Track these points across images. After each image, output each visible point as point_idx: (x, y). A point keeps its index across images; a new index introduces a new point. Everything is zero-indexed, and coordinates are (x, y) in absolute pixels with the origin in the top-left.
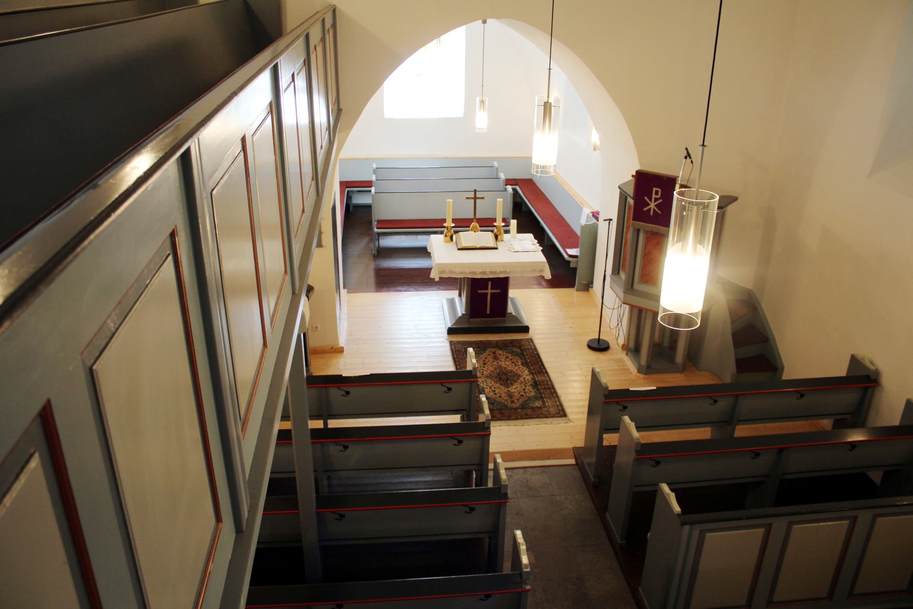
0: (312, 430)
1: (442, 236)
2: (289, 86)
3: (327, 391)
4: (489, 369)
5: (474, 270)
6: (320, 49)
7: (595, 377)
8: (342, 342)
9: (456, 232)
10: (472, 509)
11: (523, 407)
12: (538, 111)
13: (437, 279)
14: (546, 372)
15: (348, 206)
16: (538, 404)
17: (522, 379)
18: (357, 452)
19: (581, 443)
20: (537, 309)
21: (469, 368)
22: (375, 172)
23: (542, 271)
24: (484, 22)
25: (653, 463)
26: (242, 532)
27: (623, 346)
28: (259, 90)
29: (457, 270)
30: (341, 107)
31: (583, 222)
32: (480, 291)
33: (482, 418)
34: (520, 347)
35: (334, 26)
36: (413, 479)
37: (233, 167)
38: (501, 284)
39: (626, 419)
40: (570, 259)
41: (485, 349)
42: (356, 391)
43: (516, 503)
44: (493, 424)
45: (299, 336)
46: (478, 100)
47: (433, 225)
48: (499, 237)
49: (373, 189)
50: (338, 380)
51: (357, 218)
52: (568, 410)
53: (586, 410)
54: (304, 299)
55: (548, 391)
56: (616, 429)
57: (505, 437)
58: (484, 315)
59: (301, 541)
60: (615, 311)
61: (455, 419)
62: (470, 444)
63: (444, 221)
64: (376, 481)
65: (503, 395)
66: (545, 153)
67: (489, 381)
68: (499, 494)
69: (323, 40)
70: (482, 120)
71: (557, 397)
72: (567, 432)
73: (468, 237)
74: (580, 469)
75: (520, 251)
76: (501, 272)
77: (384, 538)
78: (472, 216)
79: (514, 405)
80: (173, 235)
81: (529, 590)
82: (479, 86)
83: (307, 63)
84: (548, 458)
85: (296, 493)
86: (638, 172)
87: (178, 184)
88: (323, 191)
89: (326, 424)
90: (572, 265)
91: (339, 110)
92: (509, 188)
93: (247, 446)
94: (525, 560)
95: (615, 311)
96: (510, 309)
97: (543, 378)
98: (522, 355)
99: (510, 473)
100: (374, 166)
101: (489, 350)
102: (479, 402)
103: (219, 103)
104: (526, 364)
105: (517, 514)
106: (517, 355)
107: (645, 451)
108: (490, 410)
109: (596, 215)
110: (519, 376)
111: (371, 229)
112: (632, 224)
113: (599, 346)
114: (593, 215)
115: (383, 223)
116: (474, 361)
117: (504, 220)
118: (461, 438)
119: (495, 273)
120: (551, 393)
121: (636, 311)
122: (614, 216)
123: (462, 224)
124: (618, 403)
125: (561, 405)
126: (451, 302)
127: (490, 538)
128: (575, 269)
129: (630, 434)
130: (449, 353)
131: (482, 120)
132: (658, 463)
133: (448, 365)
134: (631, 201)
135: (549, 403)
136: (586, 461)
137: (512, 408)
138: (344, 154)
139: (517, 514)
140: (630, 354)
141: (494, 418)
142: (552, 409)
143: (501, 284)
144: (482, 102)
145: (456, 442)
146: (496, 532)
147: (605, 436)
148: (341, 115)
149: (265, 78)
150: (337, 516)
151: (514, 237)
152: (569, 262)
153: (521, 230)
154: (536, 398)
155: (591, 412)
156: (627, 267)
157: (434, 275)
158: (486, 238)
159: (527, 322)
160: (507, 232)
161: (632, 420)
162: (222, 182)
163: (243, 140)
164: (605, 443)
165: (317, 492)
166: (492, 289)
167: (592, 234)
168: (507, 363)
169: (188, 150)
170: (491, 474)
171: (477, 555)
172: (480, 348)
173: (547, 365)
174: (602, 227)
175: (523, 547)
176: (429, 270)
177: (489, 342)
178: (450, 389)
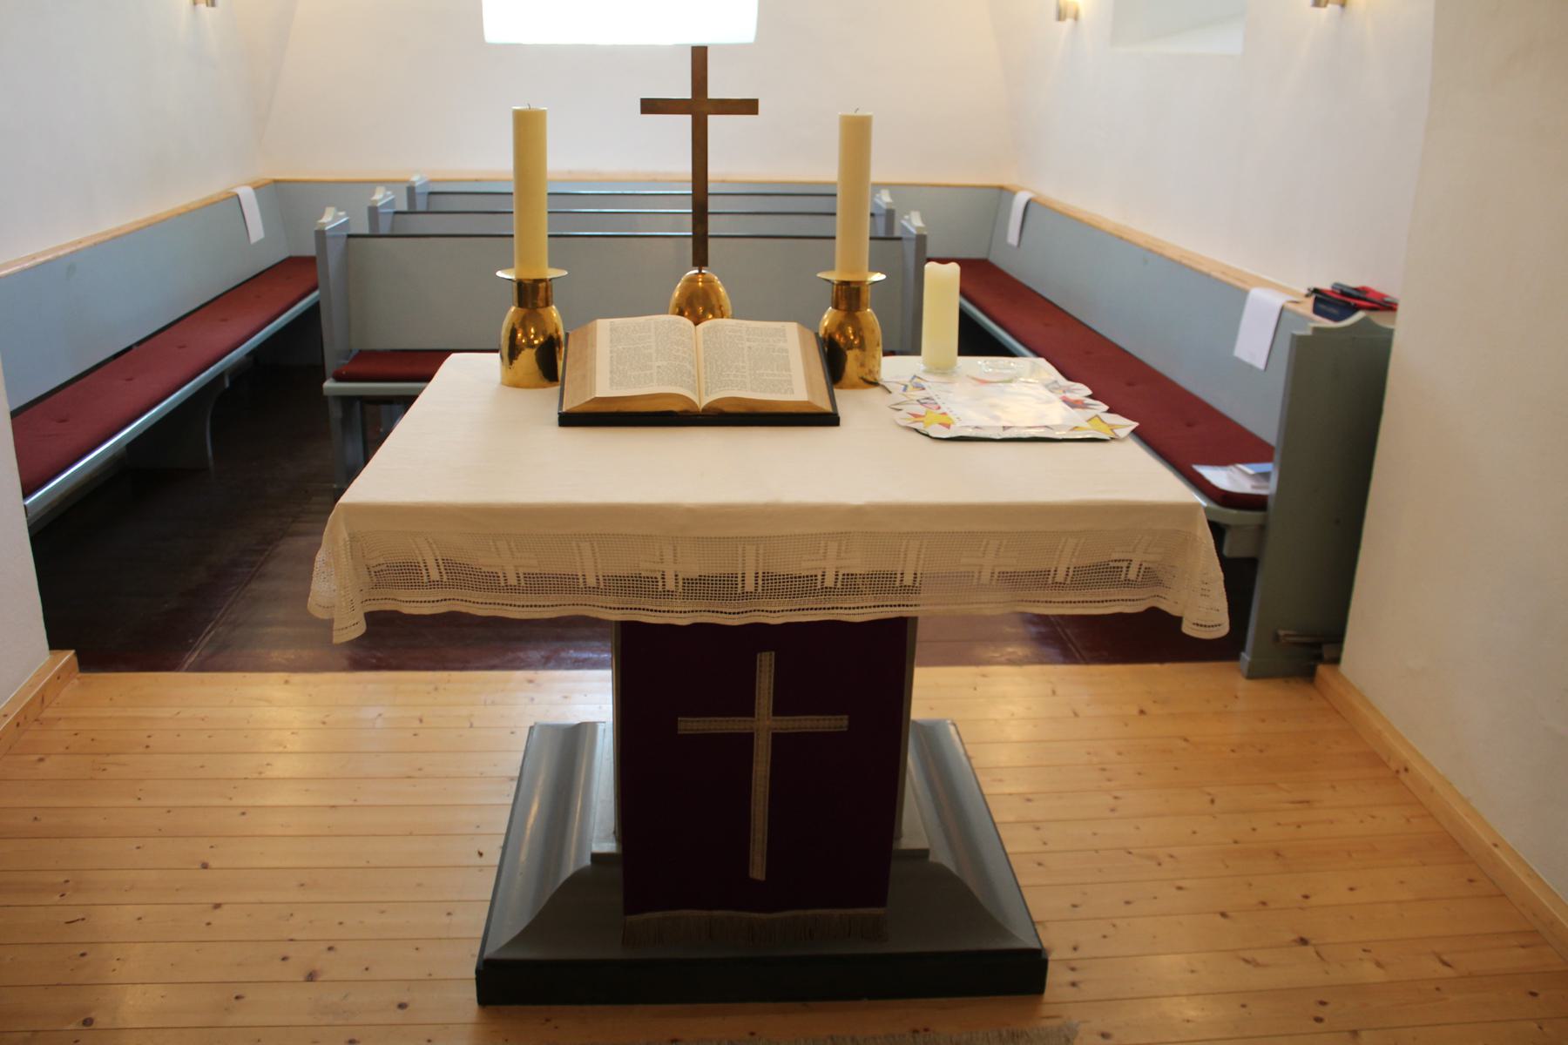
5: (646, 566)
29: (509, 563)
32: (690, 725)
76: (850, 584)
96: (916, 824)
119: (805, 585)
151: (942, 370)
160: (908, 344)
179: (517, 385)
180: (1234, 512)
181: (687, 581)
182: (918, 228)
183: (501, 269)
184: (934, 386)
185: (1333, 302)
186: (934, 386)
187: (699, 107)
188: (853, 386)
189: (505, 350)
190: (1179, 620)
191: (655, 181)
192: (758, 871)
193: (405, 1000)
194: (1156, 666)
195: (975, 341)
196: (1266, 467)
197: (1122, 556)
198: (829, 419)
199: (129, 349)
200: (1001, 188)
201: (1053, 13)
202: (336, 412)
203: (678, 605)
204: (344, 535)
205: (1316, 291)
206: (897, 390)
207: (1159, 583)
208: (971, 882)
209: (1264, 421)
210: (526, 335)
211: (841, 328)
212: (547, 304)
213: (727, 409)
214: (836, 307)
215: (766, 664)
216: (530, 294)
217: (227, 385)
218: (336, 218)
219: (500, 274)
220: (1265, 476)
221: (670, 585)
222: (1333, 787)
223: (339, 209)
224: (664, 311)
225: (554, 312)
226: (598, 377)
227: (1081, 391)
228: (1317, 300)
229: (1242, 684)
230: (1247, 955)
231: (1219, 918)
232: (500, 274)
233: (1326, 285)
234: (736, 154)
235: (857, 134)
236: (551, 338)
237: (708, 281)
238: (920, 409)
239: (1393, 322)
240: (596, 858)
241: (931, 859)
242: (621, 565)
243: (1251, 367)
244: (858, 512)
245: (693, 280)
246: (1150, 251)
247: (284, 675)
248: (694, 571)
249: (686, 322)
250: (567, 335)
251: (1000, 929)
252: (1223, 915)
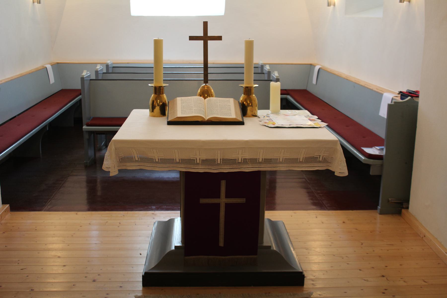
5: (191, 156)
32: (203, 201)
40: (370, 161)
76: (245, 161)
90: (373, 172)
96: (268, 239)
119: (233, 162)
152: (368, 166)
160: (267, 107)
166: (228, 196)
179: (154, 116)
180: (372, 160)
181: (203, 160)
182: (277, 76)
183: (150, 84)
184: (272, 116)
185: (403, 95)
186: (272, 116)
187: (205, 38)
188: (249, 117)
189: (151, 106)
190: (334, 172)
191: (190, 63)
192: (221, 244)
193: (122, 286)
194: (351, 211)
195: (286, 105)
196: (383, 147)
197: (317, 154)
198: (242, 123)
199: (15, 117)
200: (311, 65)
201: (326, 4)
202: (86, 136)
203: (200, 167)
204: (113, 148)
205: (401, 92)
206: (262, 118)
207: (328, 162)
208: (283, 255)
209: (381, 132)
210: (157, 102)
211: (246, 100)
212: (163, 94)
213: (213, 120)
214: (244, 94)
215: (223, 184)
216: (158, 91)
217: (48, 129)
218: (87, 74)
219: (149, 85)
220: (383, 149)
221: (198, 162)
222: (401, 241)
223: (88, 71)
224: (196, 95)
225: (165, 96)
226: (178, 112)
227: (315, 117)
228: (401, 95)
229: (378, 216)
230: (366, 279)
231: (359, 271)
232: (149, 85)
233: (404, 90)
234: (219, 55)
235: (250, 46)
236: (164, 103)
237: (208, 87)
238: (267, 121)
239: (418, 100)
241: (272, 248)
242: (185, 156)
243: (384, 118)
244: (247, 142)
245: (204, 87)
246: (356, 83)
247: (76, 212)
248: (204, 157)
249: (202, 98)
250: (168, 102)
251: (291, 267)
252: (360, 270)
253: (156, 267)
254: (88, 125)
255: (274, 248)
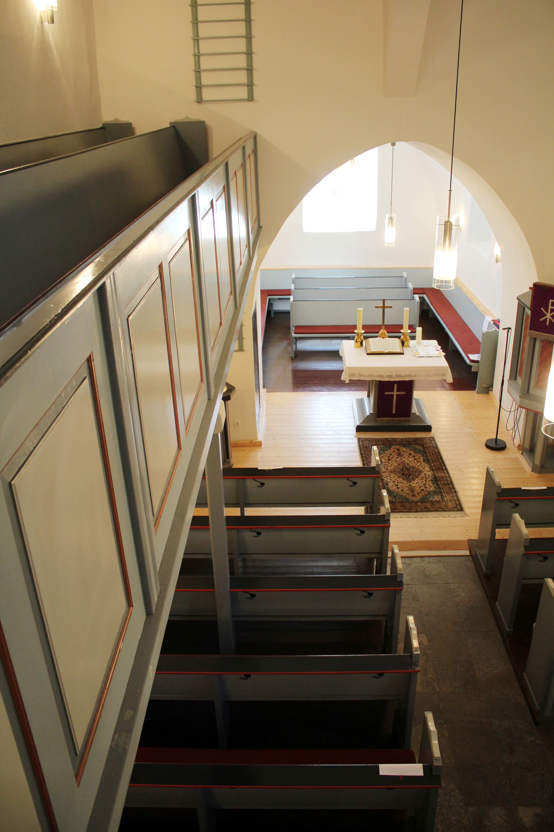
0: (228, 517)
1: (353, 341)
2: (207, 212)
3: (244, 481)
4: (393, 464)
6: (240, 175)
7: (489, 476)
8: (260, 437)
9: (366, 338)
10: (370, 594)
11: (423, 501)
12: (438, 231)
13: (347, 381)
14: (446, 469)
15: (269, 312)
16: (437, 498)
17: (423, 475)
18: (268, 537)
19: (475, 537)
20: (440, 409)
21: (373, 464)
22: (294, 281)
23: (444, 375)
24: (393, 144)
25: (542, 559)
26: (152, 614)
27: (519, 446)
28: (179, 219)
29: (366, 374)
30: (261, 224)
31: (485, 329)
32: (386, 393)
33: (383, 511)
34: (422, 445)
35: (255, 151)
36: (319, 564)
37: (150, 293)
38: (407, 387)
39: (517, 516)
40: (472, 364)
41: (390, 446)
42: (270, 483)
43: (411, 588)
44: (392, 516)
45: (215, 436)
46: (387, 217)
47: (345, 331)
48: (406, 344)
49: (291, 298)
50: (254, 473)
51: (276, 323)
52: (464, 505)
53: (481, 505)
54: (219, 402)
55: (447, 486)
56: (507, 525)
57: (404, 528)
58: (391, 415)
59: (216, 616)
60: (512, 414)
61: (359, 511)
62: (371, 535)
63: (355, 327)
64: (286, 564)
65: (405, 489)
66: (445, 269)
67: (392, 476)
68: (395, 582)
69: (243, 166)
70: (390, 236)
71: (455, 492)
72: (462, 526)
73: (377, 343)
74: (473, 560)
75: (426, 355)
76: (406, 376)
77: (287, 616)
78: (380, 323)
79: (415, 499)
80: (89, 360)
81: (418, 671)
82: (389, 203)
83: (227, 190)
84: (445, 549)
85: (212, 573)
86: (535, 285)
87: (94, 315)
88: (241, 305)
89: (242, 512)
91: (260, 228)
92: (417, 297)
93: (157, 542)
94: (415, 643)
95: (512, 414)
96: (414, 409)
97: (442, 474)
98: (424, 453)
99: (407, 561)
100: (294, 276)
101: (393, 447)
102: (381, 494)
103: (124, 248)
104: (427, 461)
105: (414, 599)
106: (420, 452)
107: (533, 545)
108: (391, 502)
109: (496, 323)
110: (421, 472)
111: (289, 333)
112: (529, 334)
113: (496, 446)
114: (494, 323)
115: (301, 329)
116: (378, 458)
117: (411, 327)
118: (363, 529)
119: (400, 376)
120: (450, 489)
121: (531, 415)
122: (512, 324)
123: (372, 330)
124: (510, 501)
125: (458, 500)
126: (360, 402)
127: (386, 621)
128: (476, 373)
129: (520, 531)
130: (357, 449)
131: (390, 236)
132: (546, 558)
133: (356, 462)
134: (528, 312)
135: (447, 497)
136: (479, 552)
137: (412, 502)
138: (264, 265)
139: (414, 599)
140: (525, 454)
141: (394, 509)
142: (449, 504)
143: (407, 387)
144: (391, 218)
145: (358, 532)
146: (392, 615)
147: (497, 530)
148: (261, 231)
149: (184, 208)
150: (249, 596)
151: (419, 344)
152: (470, 367)
153: (426, 336)
154: (435, 493)
155: (485, 507)
156: (523, 373)
157: (345, 377)
158: (394, 344)
159: (429, 420)
160: (413, 338)
161: (522, 519)
162: (139, 308)
163: (160, 267)
164: (498, 537)
165: (232, 573)
167: (493, 341)
168: (410, 459)
169: (104, 284)
170: (389, 561)
171: (375, 636)
172: (385, 445)
173: (446, 463)
174: (502, 335)
175: (414, 632)
176: (340, 372)
177: (394, 440)
178: (355, 483)
192: (394, 412)
198: (403, 354)
215: (396, 386)
229: (476, 395)
240: (370, 414)
244: (407, 367)
248: (388, 374)
251: (425, 423)
253: (362, 423)
254: (295, 333)
255: (417, 414)
